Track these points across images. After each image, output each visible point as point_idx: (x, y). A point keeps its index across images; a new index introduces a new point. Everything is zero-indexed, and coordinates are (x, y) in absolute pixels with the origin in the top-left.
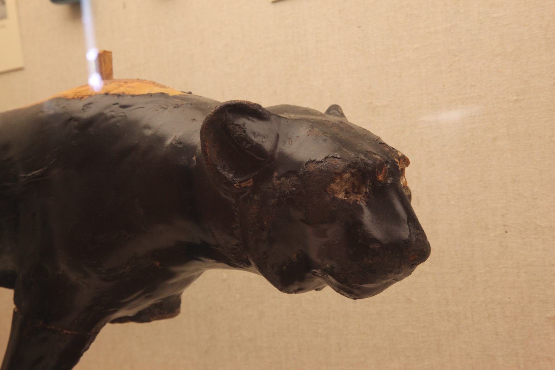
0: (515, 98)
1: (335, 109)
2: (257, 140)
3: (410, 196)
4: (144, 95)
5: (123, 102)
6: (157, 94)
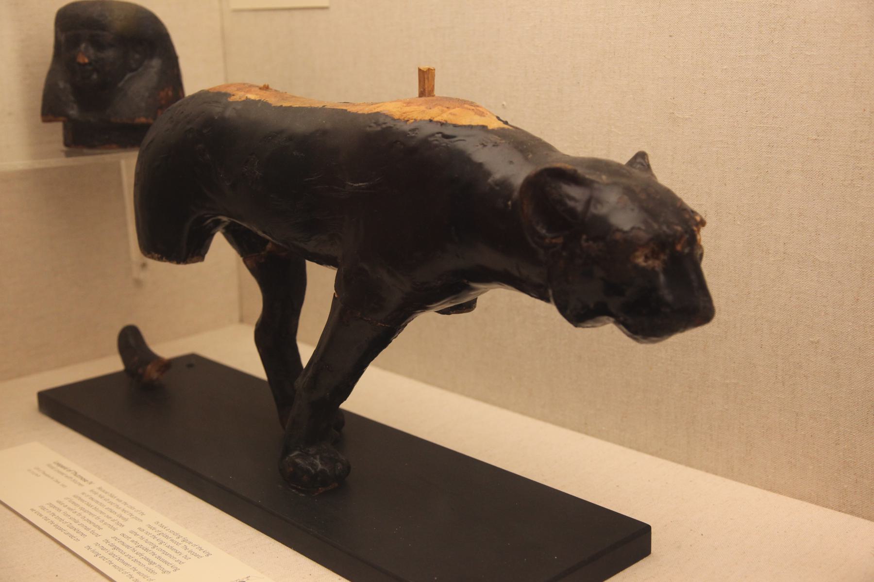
0: (815, 137)
1: (641, 158)
2: (571, 204)
3: (701, 255)
4: (465, 126)
5: (447, 133)
6: (478, 126)
